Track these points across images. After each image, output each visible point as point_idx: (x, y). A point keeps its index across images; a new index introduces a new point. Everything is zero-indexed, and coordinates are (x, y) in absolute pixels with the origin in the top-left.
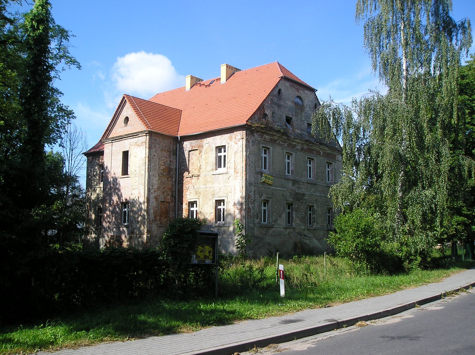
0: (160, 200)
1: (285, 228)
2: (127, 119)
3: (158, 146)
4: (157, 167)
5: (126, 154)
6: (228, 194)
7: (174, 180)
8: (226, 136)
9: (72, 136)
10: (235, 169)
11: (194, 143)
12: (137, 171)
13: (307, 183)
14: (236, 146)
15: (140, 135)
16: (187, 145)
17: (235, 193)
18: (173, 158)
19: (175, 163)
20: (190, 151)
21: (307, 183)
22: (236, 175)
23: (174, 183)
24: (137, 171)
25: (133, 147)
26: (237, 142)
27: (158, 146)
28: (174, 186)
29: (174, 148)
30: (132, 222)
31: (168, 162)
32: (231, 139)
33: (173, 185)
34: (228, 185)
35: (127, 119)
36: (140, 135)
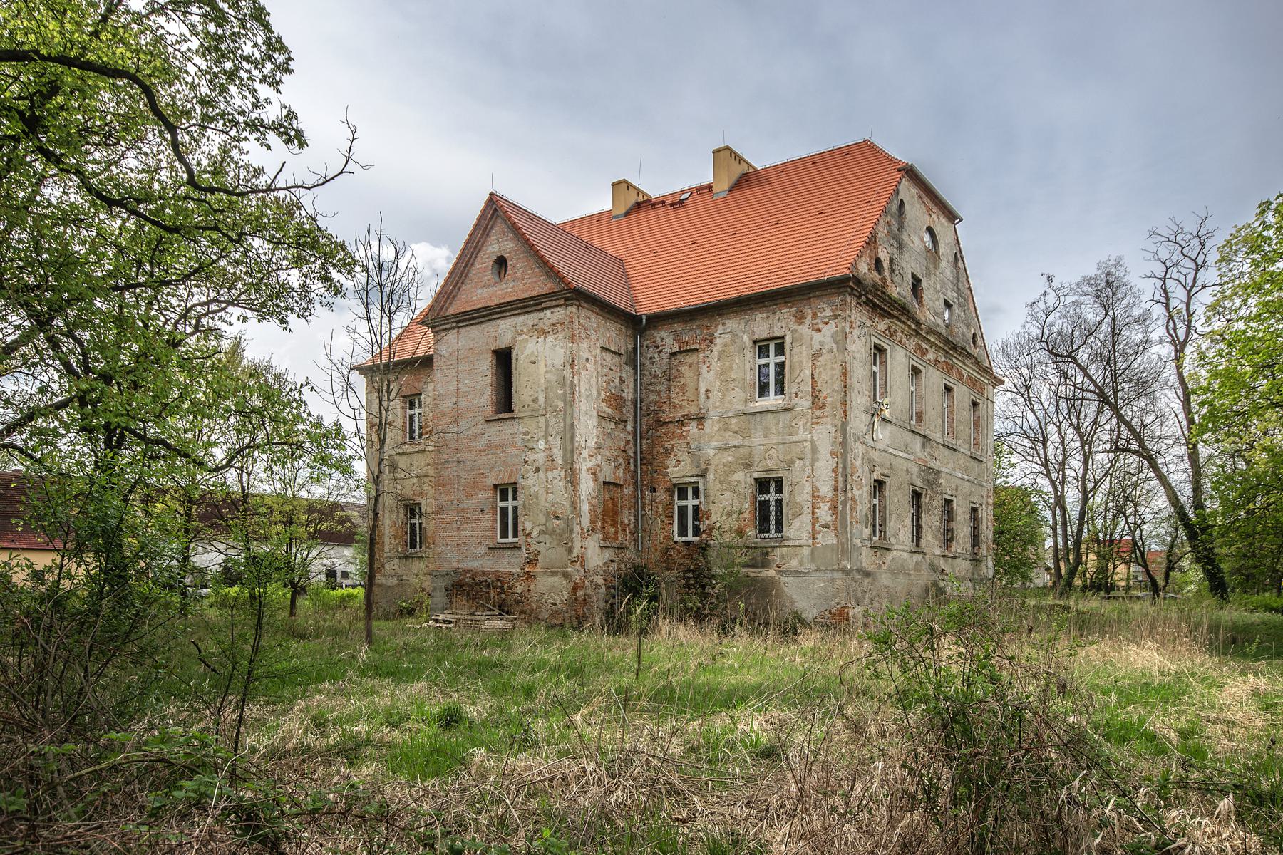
0: (602, 479)
1: (911, 552)
2: (501, 263)
3: (594, 336)
4: (595, 392)
5: (503, 358)
6: (793, 462)
7: (629, 428)
8: (787, 312)
9: (384, 277)
10: (815, 397)
11: (687, 332)
12: (541, 399)
13: (944, 445)
14: (818, 336)
15: (549, 304)
16: (666, 338)
17: (814, 461)
18: (627, 373)
19: (631, 385)
20: (673, 354)
21: (944, 445)
22: (818, 412)
23: (630, 438)
24: (541, 399)
25: (524, 337)
26: (821, 326)
27: (594, 336)
28: (631, 445)
29: (630, 347)
30: (529, 535)
31: (617, 381)
32: (800, 318)
33: (627, 442)
34: (794, 439)
35: (501, 263)
36: (549, 304)
